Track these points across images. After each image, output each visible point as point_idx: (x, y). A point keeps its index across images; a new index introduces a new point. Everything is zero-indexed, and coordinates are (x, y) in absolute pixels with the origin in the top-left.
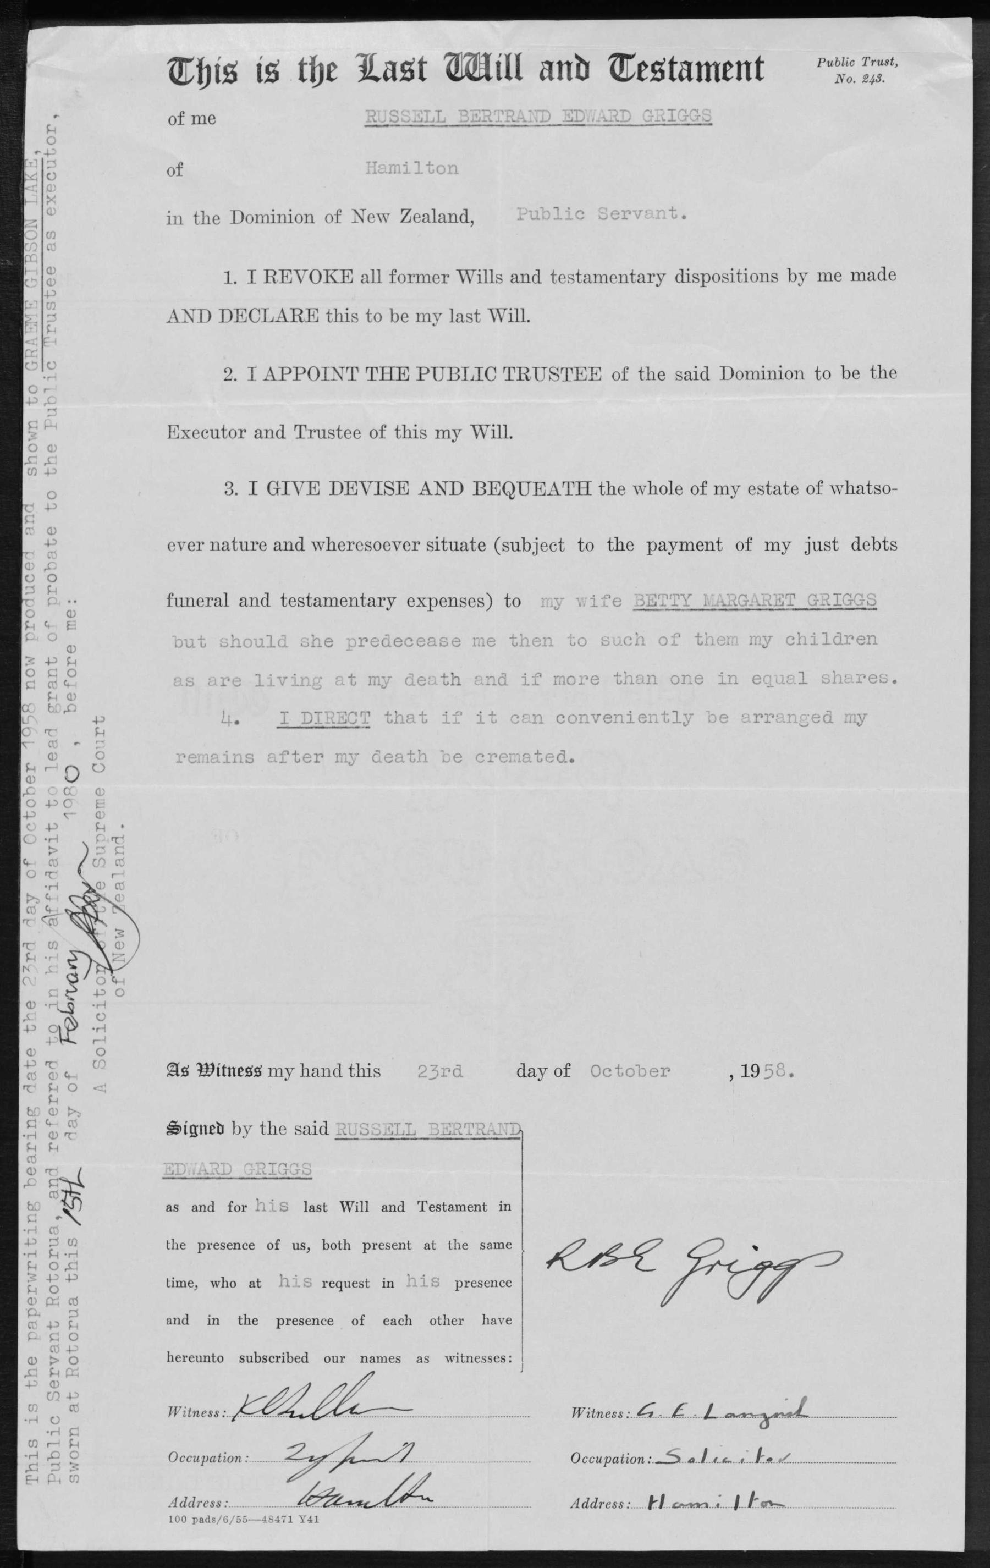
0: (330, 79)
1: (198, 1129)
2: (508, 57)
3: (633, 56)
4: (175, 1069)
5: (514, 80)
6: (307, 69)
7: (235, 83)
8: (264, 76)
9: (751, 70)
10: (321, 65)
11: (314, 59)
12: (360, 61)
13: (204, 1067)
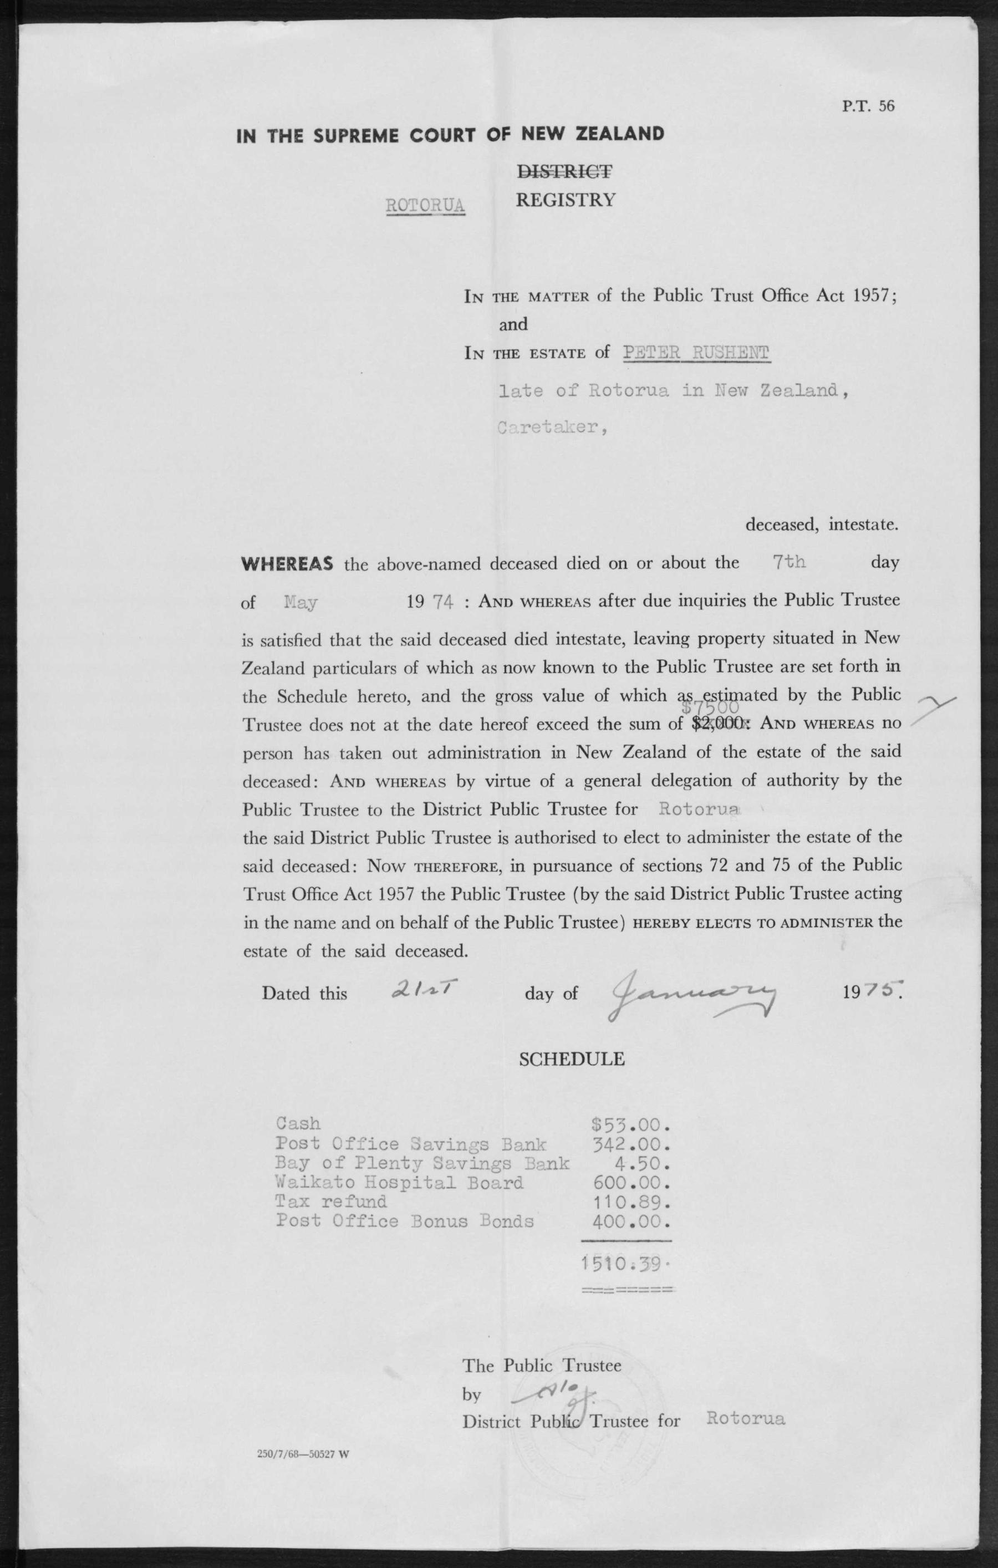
6: (287, 973)
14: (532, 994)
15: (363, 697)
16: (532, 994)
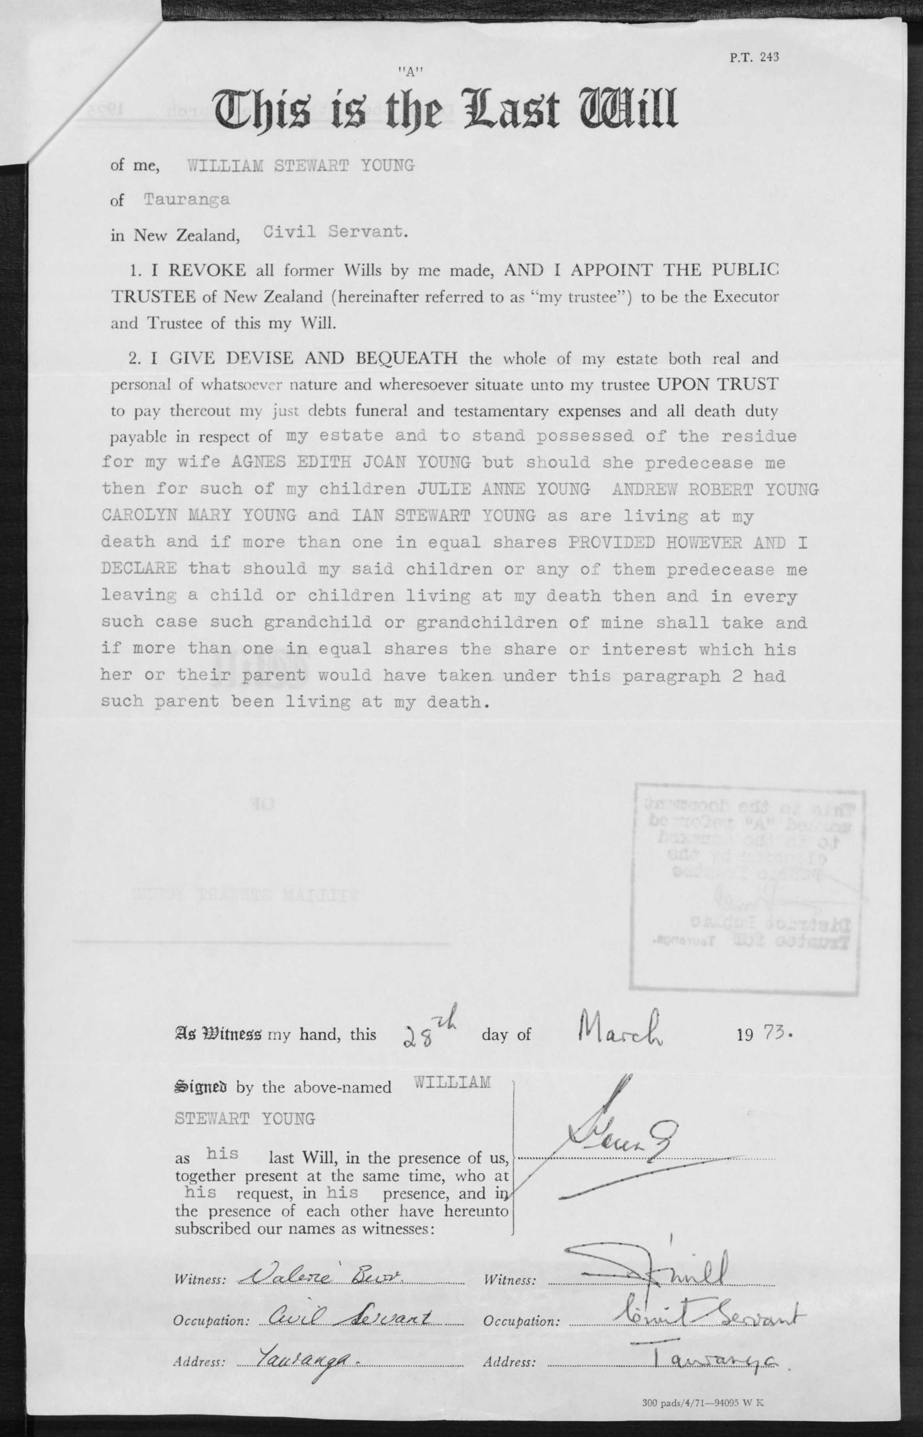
0: (430, 124)
1: (203, 1087)
2: (657, 95)
3: (463, 92)
4: (182, 1032)
5: (666, 127)
6: (399, 109)
7: (362, 126)
8: (344, 118)
9: (661, 110)
10: (417, 103)
11: (406, 94)
12: (469, 97)
13: (210, 1030)
14: (489, 1035)
15: (343, 298)
16: (489, 1035)
